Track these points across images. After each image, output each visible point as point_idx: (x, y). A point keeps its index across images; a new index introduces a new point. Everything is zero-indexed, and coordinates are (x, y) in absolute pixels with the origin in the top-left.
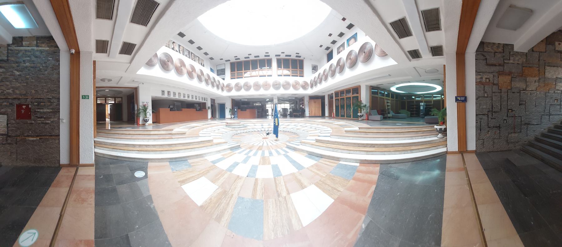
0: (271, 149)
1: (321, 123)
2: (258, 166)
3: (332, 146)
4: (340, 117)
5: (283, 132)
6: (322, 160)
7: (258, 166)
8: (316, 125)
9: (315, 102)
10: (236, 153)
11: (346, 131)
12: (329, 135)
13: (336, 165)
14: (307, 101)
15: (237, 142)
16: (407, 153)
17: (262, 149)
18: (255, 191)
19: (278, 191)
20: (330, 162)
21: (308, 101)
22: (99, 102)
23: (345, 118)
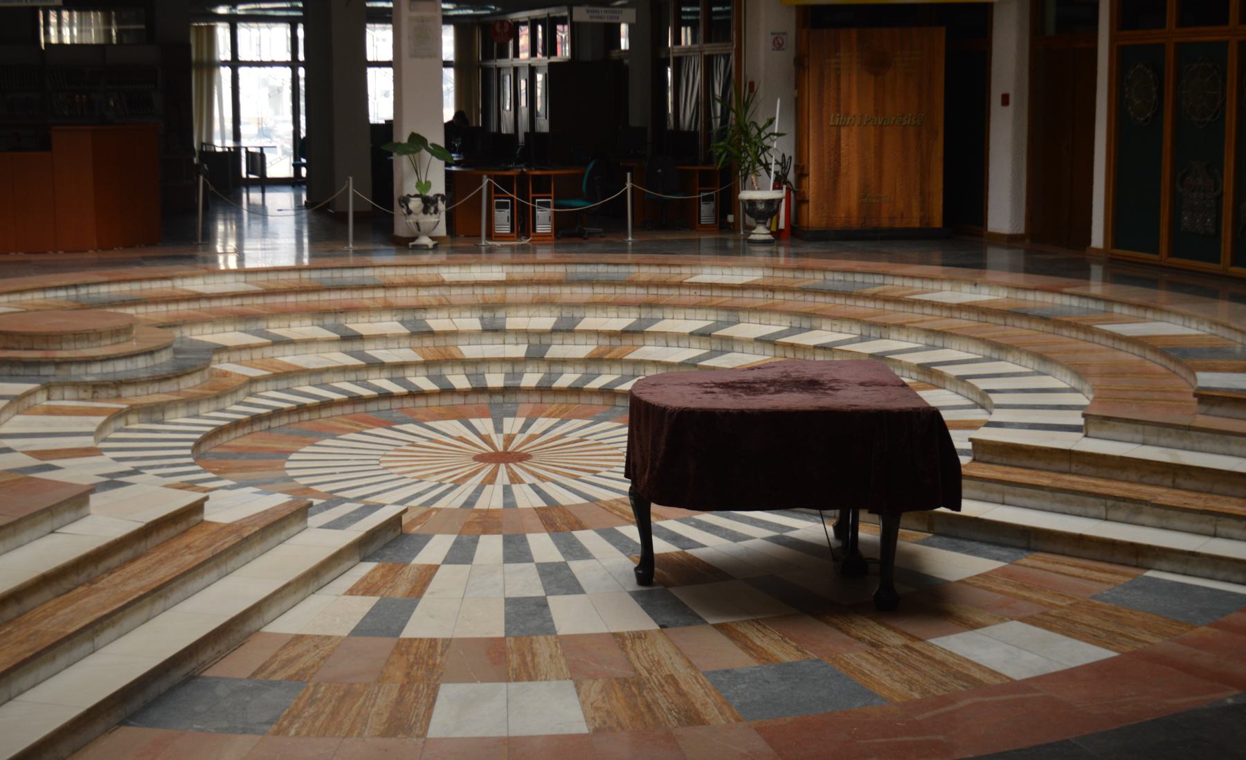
1: (964, 322)
2: (537, 565)
3: (1097, 486)
4: (1225, 265)
5: (597, 400)
6: (1032, 562)
7: (537, 565)
8: (921, 341)
9: (876, 65)
10: (396, 503)
11: (1207, 398)
12: (1077, 419)
13: (1128, 579)
14: (778, 45)
15: (601, 444)
16: (1210, 529)
18: (752, 649)
19: (898, 655)
20: (1084, 568)
21: (791, 39)
22: (505, 229)
23: (1225, 265)
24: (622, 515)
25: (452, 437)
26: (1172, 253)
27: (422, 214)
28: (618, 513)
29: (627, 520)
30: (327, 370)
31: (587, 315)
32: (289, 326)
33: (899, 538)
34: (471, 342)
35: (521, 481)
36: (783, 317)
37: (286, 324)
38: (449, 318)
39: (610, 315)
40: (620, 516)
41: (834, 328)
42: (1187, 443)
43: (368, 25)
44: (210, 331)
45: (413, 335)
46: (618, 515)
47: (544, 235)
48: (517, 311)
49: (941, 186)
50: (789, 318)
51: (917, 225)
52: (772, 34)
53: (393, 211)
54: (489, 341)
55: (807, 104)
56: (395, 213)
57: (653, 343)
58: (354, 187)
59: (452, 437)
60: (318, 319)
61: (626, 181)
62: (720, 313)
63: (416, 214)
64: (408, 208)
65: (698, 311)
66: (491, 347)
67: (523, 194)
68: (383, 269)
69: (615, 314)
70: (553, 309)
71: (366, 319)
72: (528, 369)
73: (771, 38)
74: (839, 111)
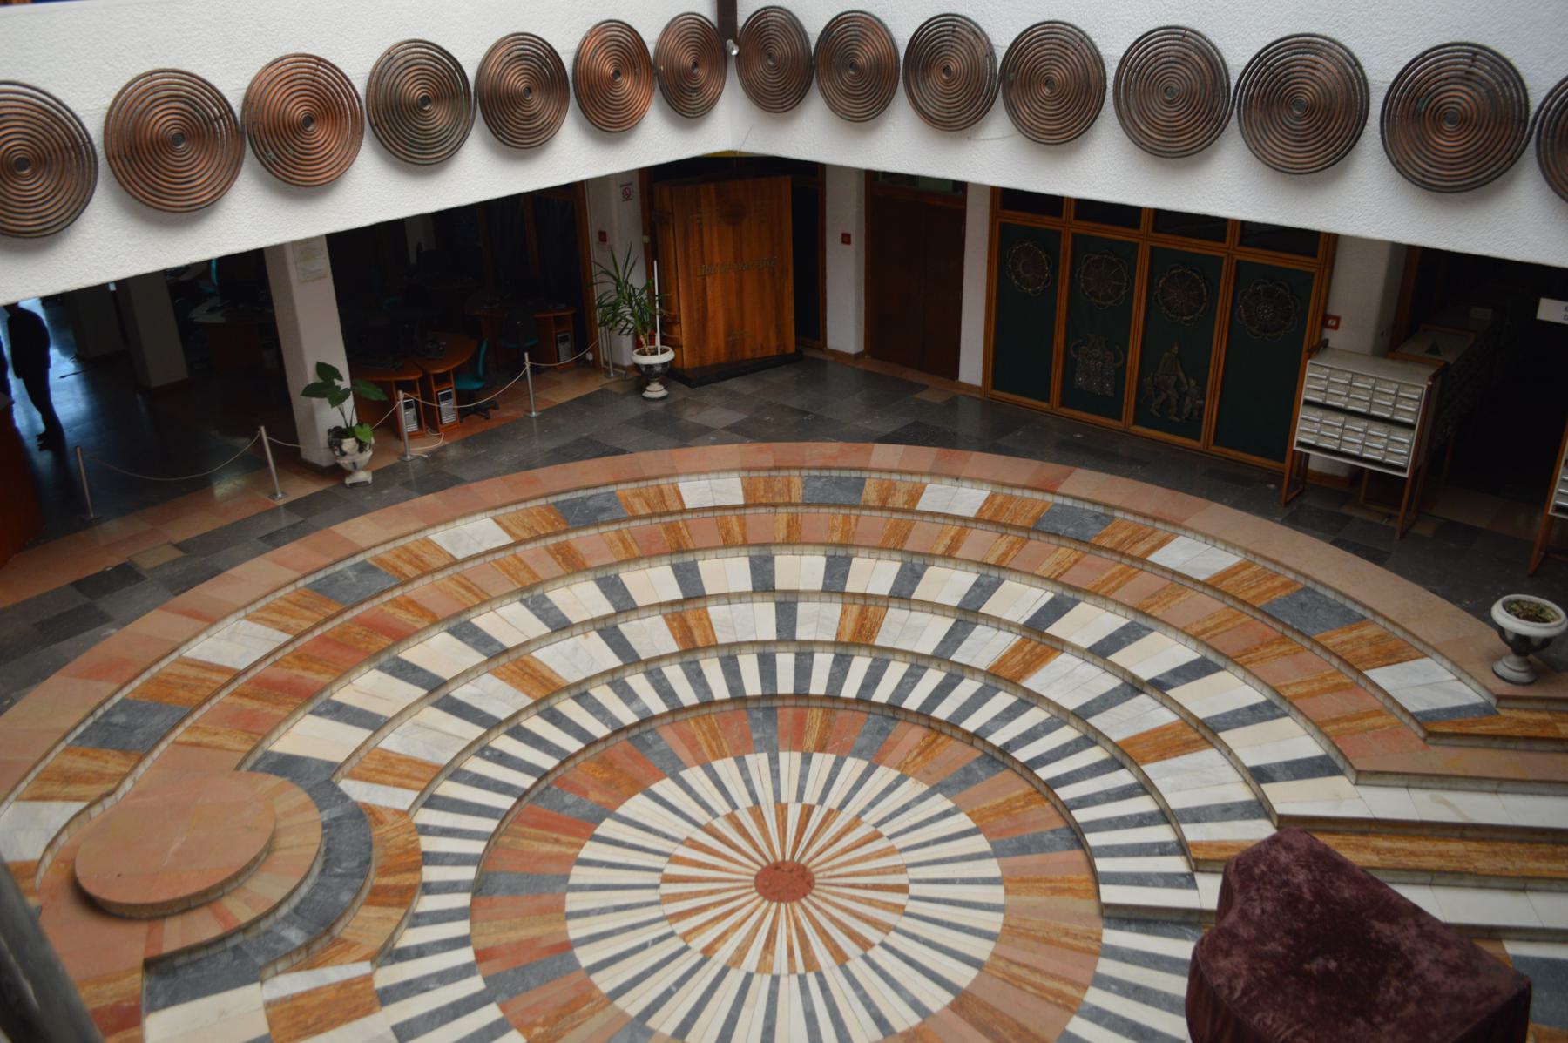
0: (1069, 990)
25: (674, 839)
26: (1063, 404)
27: (358, 454)
28: (1030, 989)
32: (350, 682)
35: (872, 945)
36: (817, 548)
38: (492, 610)
39: (642, 566)
41: (872, 555)
42: (1446, 785)
45: (492, 657)
47: (451, 425)
49: (792, 317)
50: (823, 548)
51: (775, 353)
52: (621, 186)
53: (297, 443)
55: (673, 263)
56: (301, 446)
57: (715, 603)
58: (268, 435)
61: (524, 360)
62: (751, 549)
63: (352, 455)
64: (341, 451)
65: (729, 550)
66: (561, 643)
67: (427, 395)
68: (373, 550)
70: (587, 573)
71: (416, 641)
73: (620, 190)
74: (703, 262)
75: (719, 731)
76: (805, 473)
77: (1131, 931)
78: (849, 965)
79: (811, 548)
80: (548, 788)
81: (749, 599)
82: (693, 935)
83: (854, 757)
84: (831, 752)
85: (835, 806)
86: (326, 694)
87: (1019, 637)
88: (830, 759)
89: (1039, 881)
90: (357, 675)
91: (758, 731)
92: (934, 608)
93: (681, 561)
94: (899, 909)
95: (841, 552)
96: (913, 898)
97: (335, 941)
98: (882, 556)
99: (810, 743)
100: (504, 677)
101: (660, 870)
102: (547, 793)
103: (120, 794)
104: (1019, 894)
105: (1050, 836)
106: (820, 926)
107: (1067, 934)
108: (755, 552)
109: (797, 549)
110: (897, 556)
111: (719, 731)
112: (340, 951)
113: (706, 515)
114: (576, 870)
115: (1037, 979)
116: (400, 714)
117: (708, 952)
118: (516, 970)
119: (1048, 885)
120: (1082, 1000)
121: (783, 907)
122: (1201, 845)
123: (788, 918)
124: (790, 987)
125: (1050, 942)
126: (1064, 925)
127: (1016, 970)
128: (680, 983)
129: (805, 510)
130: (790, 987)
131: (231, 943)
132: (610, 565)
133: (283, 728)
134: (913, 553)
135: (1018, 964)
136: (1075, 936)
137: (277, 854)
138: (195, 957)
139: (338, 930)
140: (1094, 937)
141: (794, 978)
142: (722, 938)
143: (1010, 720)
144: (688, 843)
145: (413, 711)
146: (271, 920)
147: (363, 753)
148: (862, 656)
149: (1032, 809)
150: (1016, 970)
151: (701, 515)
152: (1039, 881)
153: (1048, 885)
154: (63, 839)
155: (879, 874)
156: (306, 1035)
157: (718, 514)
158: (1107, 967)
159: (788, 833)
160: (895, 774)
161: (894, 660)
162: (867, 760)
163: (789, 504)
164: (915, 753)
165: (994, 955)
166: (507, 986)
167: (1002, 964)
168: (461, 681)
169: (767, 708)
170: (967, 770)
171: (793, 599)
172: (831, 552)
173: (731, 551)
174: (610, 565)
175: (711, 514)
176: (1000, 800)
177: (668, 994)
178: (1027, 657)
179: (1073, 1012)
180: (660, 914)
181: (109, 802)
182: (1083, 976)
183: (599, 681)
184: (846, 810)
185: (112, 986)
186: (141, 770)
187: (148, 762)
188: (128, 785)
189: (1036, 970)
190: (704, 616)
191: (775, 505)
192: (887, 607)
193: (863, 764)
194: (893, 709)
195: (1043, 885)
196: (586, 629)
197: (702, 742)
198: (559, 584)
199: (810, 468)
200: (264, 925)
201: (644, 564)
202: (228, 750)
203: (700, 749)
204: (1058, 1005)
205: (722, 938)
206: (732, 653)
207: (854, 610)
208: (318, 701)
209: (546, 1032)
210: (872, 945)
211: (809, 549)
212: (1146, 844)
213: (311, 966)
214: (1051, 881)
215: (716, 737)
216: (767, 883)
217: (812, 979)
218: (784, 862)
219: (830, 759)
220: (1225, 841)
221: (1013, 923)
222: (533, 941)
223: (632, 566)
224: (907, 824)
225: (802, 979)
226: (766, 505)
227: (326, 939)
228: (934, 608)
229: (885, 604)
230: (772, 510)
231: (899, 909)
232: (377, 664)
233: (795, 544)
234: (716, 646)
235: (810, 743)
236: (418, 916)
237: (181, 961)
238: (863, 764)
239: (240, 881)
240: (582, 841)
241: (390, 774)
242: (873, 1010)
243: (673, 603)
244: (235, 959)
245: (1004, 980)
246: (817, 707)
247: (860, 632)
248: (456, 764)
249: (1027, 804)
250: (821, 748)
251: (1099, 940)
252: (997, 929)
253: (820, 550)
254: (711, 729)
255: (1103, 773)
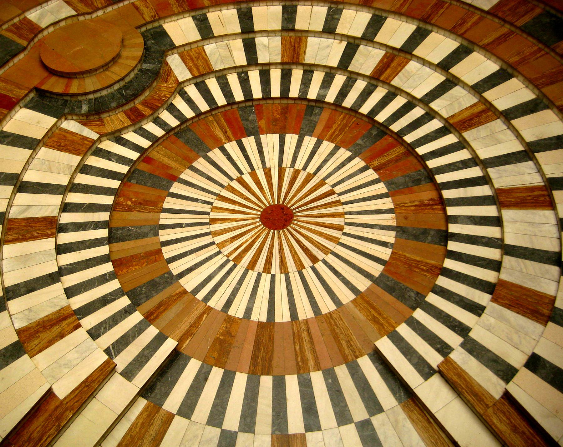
0: (311, 363)
17: (270, 366)
24: (298, 351)
25: (263, 161)
28: (297, 347)
29: (424, 209)
30: (225, 69)
31: (389, 16)
33: (39, 24)
34: (316, 36)
37: (219, 9)
39: (402, 19)
40: (296, 352)
43: (387, 260)
44: (176, 18)
46: (295, 349)
48: (350, 7)
54: (326, 36)
57: (416, 60)
59: (263, 161)
60: (237, 5)
69: (405, 20)
70: (371, 9)
72: (339, 73)
75: (347, 128)
76: (548, 9)
77: (376, 368)
78: (250, 272)
79: (495, 58)
80: (251, 106)
81: (434, 68)
82: (216, 210)
83: (385, 184)
84: (379, 174)
85: (342, 201)
86: (204, 11)
87: (543, 184)
88: (376, 176)
89: (374, 309)
90: (225, 8)
91: (362, 140)
92: (518, 136)
93: (424, 27)
94: (300, 267)
95: (510, 71)
96: (314, 269)
97: (101, 120)
98: (368, 45)
99: (376, 163)
100: (284, 42)
101: (241, 173)
102: (248, 109)
103: (94, 16)
104: (356, 307)
105: (412, 294)
106: (263, 248)
107: (348, 342)
108: (465, 43)
109: (488, 54)
110: (537, 92)
111: (347, 128)
112: (97, 125)
113: (464, 6)
114: (217, 150)
115: (307, 346)
116: (222, 36)
117: (214, 221)
118: (150, 174)
119: (375, 314)
120: (309, 372)
121: (262, 226)
122: (452, 364)
123: (257, 233)
124: (220, 259)
125: (336, 337)
126: (354, 337)
127: (305, 335)
128: (188, 225)
129: (520, 33)
130: (220, 259)
131: (65, 98)
132: (385, 11)
133: (174, 18)
134: (545, 95)
135: (309, 334)
136: (350, 345)
137: (107, 72)
138: (52, 96)
139: (104, 116)
140: (357, 353)
141: (226, 258)
142: (224, 220)
143: (476, 224)
144: (267, 171)
145: (231, 38)
146: (84, 98)
147: (194, 46)
148: (455, 136)
149: (425, 275)
150: (305, 335)
151: (461, 5)
152: (374, 309)
153: (375, 314)
154: (63, 24)
155: (316, 246)
156: (57, 148)
157: (471, 9)
158: (342, 372)
159: (307, 198)
160: (391, 206)
161: (467, 149)
162: (389, 190)
163: (512, 24)
164: (414, 204)
165: (306, 321)
166: (141, 178)
167: (303, 327)
168: (265, 34)
169: (382, 131)
170: (425, 232)
171: (456, 82)
172: (505, 67)
173: (453, 36)
174: (385, 11)
175: (467, 8)
176: (417, 258)
177: (180, 226)
178: (530, 198)
179: (298, 373)
180: (218, 192)
181: (88, 17)
182: (326, 363)
183: (322, 69)
184: (345, 206)
185: (18, 90)
186: (110, 9)
187: (115, 7)
188: (100, 13)
189: (311, 342)
190: (403, 64)
191: (505, 21)
192: (498, 118)
193: (385, 190)
194: (431, 174)
195: (373, 312)
196: (343, 38)
197: (334, 128)
198: (354, 8)
199: (552, 7)
200: (80, 98)
201: (404, 19)
202: (143, 17)
203: (328, 131)
204: (297, 364)
205: (224, 220)
206: (396, 92)
207: (481, 107)
208: (199, 13)
209: (130, 205)
210: (269, 272)
211: (494, 58)
212: (439, 338)
213: (84, 124)
214: (380, 314)
215: (341, 130)
216: (270, 212)
217: (231, 264)
218: (289, 208)
219: (376, 176)
220: (467, 374)
221: (334, 316)
222: (169, 167)
223: (397, 17)
224: (360, 234)
225: (228, 261)
226: (500, 18)
227: (97, 117)
228: (518, 136)
229: (499, 116)
230: (502, 23)
231: (300, 267)
232: (239, 7)
233: (487, 51)
234: (389, 84)
235: (376, 163)
236: (141, 128)
237: (48, 95)
238: (385, 190)
239: (85, 76)
240: (233, 139)
241: (193, 61)
242: (232, 297)
243: (394, 49)
244: (62, 105)
245: (294, 333)
246: (405, 147)
247: (464, 122)
248: (224, 72)
249: (427, 271)
250: (376, 169)
251: (357, 357)
252: (324, 311)
253: (500, 63)
254: (345, 125)
255: (476, 288)
